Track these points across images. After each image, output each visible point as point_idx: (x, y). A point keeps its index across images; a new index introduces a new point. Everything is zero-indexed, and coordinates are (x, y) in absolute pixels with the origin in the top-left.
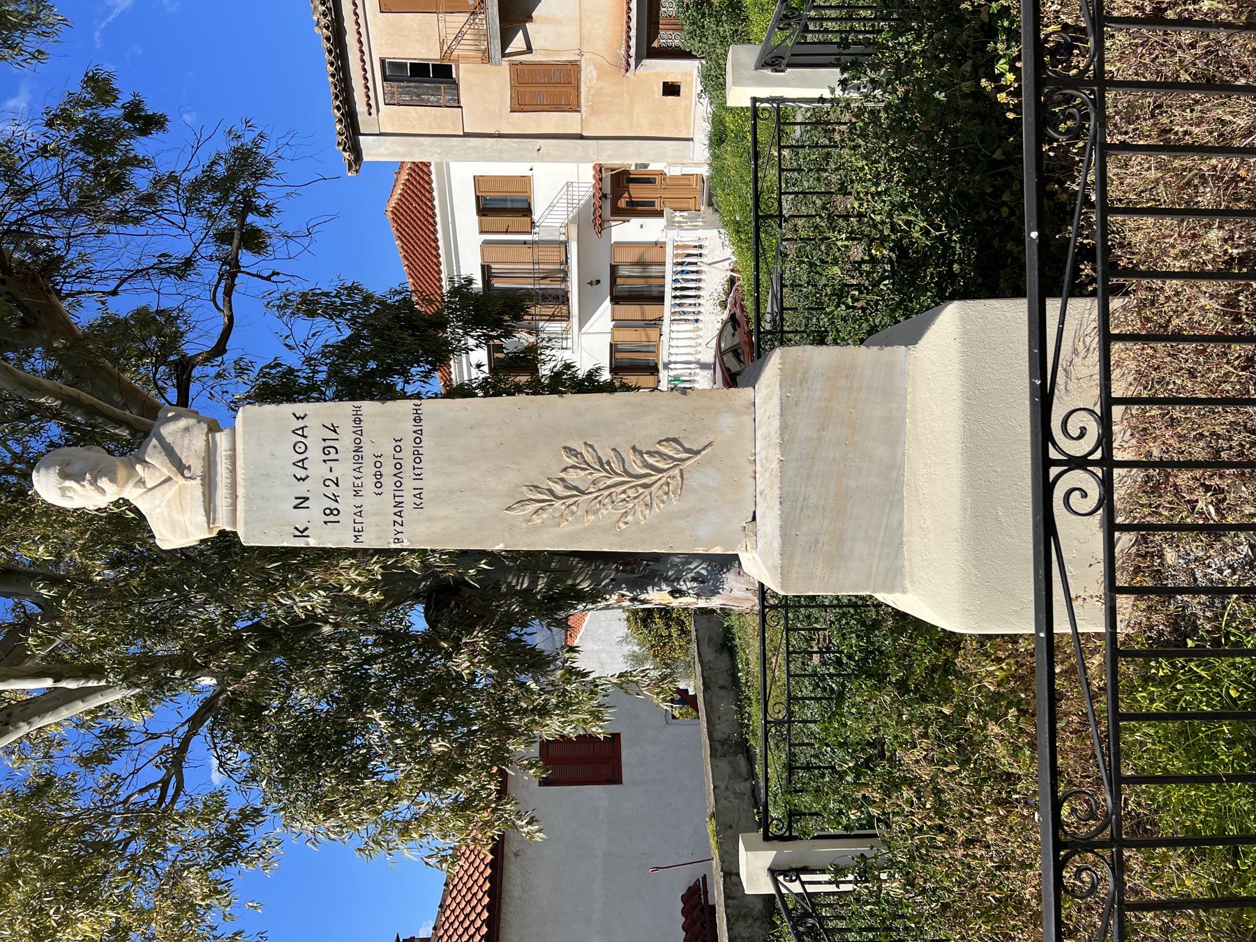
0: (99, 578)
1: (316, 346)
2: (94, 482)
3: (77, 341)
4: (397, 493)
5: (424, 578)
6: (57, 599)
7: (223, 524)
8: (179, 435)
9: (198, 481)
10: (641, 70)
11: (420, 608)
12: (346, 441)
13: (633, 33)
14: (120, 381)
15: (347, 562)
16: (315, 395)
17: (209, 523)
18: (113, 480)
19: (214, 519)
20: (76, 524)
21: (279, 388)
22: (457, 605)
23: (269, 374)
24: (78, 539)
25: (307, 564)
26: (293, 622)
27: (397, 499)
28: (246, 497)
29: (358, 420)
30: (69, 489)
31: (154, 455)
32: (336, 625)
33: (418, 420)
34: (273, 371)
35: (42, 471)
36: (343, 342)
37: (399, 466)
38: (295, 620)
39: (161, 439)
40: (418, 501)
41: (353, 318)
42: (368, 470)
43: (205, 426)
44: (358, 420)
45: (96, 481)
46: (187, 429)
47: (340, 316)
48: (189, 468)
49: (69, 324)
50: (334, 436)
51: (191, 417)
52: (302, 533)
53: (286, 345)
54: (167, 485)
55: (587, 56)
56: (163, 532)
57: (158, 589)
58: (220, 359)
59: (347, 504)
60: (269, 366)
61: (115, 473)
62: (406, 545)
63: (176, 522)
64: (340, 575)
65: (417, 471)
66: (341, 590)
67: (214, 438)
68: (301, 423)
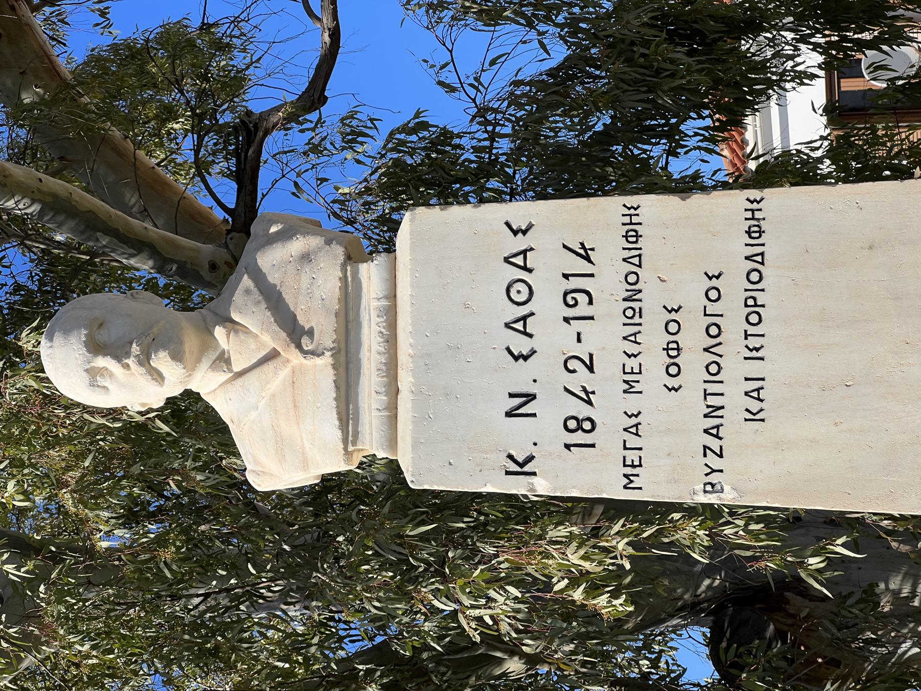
0: (105, 544)
1: (498, 83)
2: (144, 360)
3: (63, 89)
4: (712, 388)
5: (709, 571)
6: (32, 584)
7: (372, 444)
8: (291, 269)
9: (326, 361)
11: (699, 633)
12: (608, 281)
14: (135, 164)
15: (562, 532)
16: (493, 183)
17: (345, 441)
18: (177, 356)
19: (356, 434)
20: (69, 440)
21: (431, 172)
22: (780, 635)
23: (403, 143)
24: (68, 468)
25: (482, 529)
26: (452, 648)
27: (712, 401)
28: (416, 392)
29: (632, 235)
30: (102, 371)
31: (248, 311)
32: (532, 660)
33: (755, 232)
34: (414, 138)
35: (58, 339)
36: (551, 73)
37: (714, 331)
38: (459, 645)
39: (259, 277)
40: (755, 406)
41: (572, 24)
42: (653, 337)
43: (339, 251)
44: (632, 235)
45: (148, 358)
46: (306, 258)
47: (547, 19)
48: (310, 333)
49: (48, 57)
50: (585, 267)
51: (314, 234)
52: (522, 466)
53: (441, 83)
54: (269, 367)
56: (262, 458)
57: (205, 569)
58: (313, 116)
59: (609, 410)
60: (405, 129)
61: (181, 343)
62: (728, 497)
63: (284, 439)
64: (548, 556)
65: (753, 342)
66: (548, 587)
67: (356, 273)
68: (521, 243)
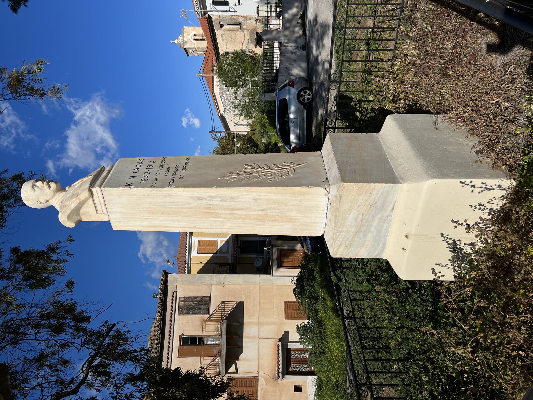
10: (284, 380)
13: (280, 362)
55: (261, 374)
